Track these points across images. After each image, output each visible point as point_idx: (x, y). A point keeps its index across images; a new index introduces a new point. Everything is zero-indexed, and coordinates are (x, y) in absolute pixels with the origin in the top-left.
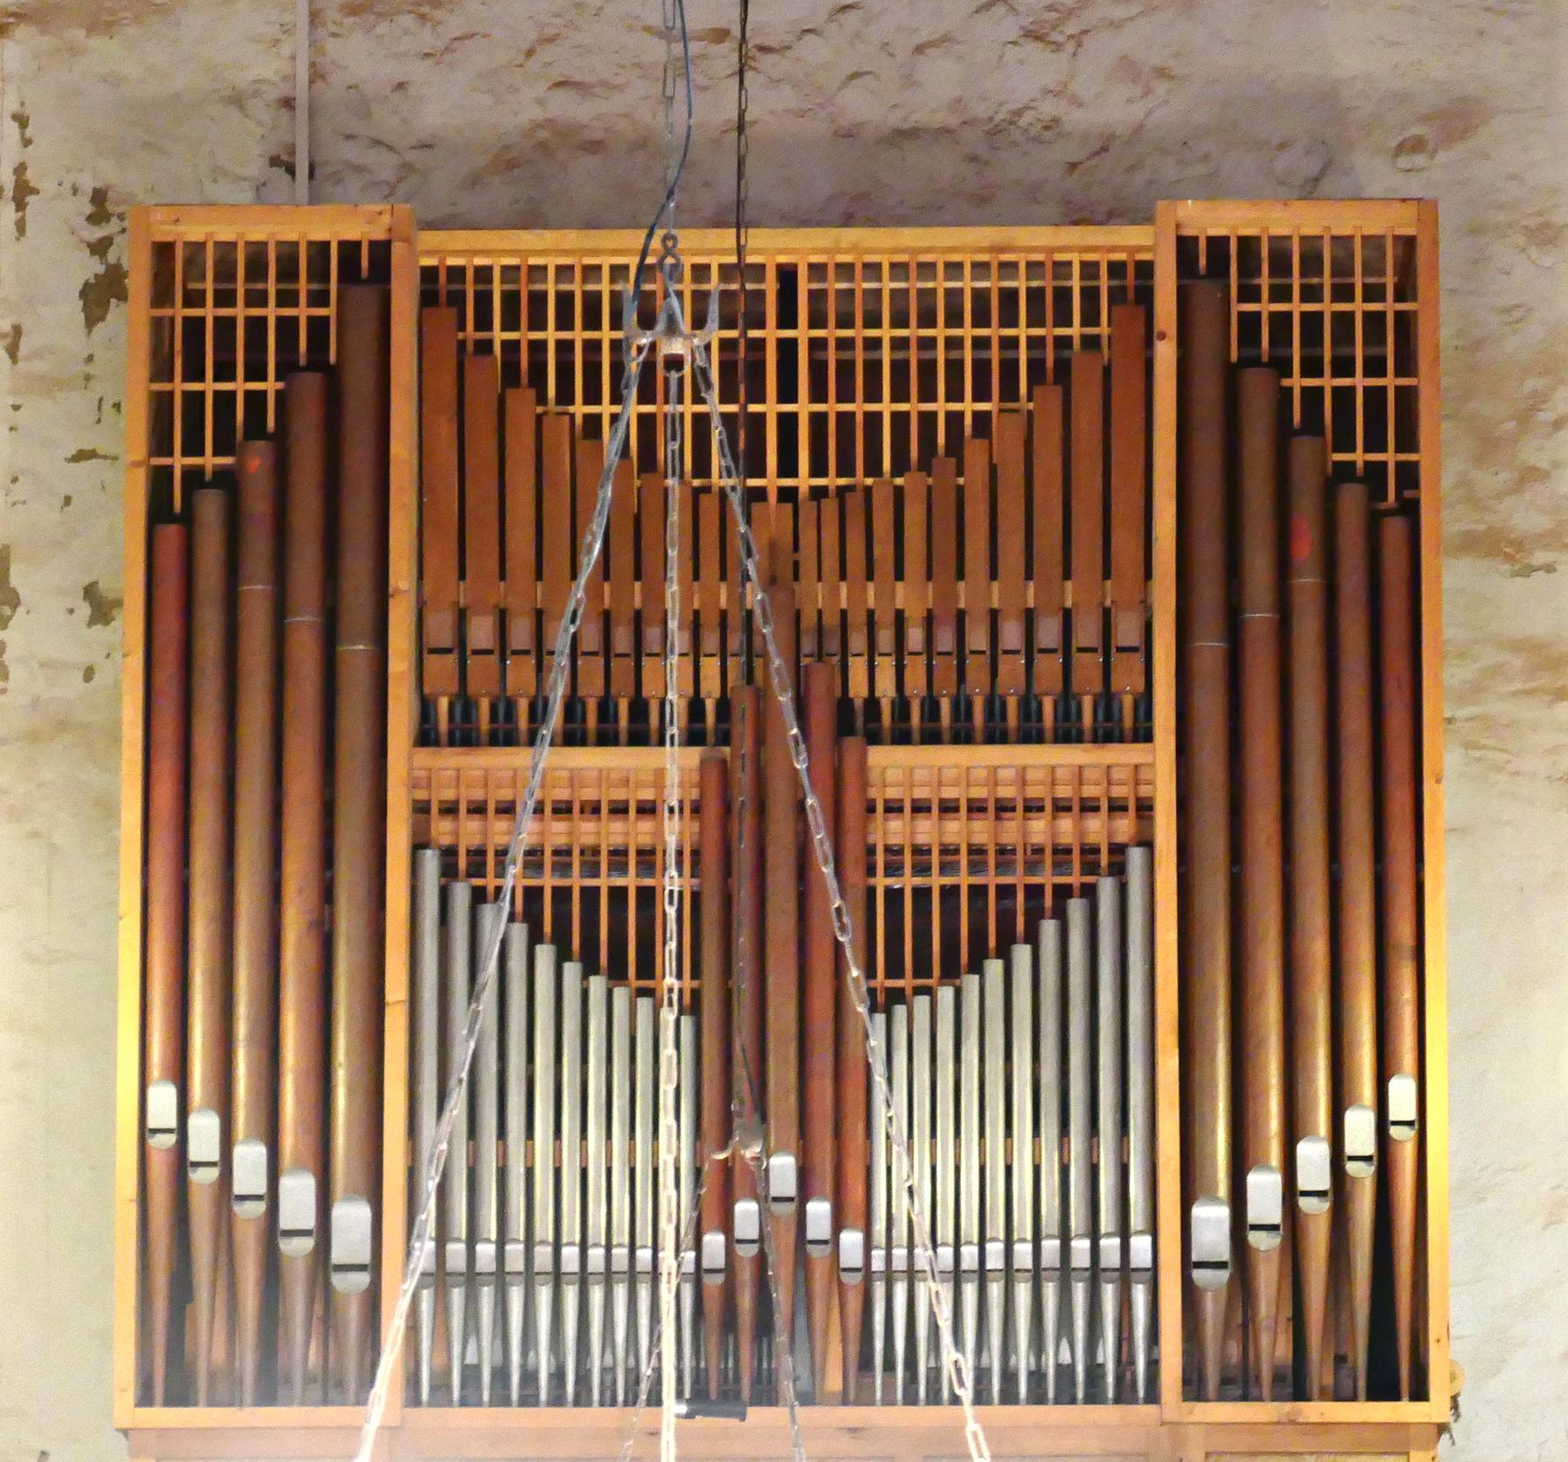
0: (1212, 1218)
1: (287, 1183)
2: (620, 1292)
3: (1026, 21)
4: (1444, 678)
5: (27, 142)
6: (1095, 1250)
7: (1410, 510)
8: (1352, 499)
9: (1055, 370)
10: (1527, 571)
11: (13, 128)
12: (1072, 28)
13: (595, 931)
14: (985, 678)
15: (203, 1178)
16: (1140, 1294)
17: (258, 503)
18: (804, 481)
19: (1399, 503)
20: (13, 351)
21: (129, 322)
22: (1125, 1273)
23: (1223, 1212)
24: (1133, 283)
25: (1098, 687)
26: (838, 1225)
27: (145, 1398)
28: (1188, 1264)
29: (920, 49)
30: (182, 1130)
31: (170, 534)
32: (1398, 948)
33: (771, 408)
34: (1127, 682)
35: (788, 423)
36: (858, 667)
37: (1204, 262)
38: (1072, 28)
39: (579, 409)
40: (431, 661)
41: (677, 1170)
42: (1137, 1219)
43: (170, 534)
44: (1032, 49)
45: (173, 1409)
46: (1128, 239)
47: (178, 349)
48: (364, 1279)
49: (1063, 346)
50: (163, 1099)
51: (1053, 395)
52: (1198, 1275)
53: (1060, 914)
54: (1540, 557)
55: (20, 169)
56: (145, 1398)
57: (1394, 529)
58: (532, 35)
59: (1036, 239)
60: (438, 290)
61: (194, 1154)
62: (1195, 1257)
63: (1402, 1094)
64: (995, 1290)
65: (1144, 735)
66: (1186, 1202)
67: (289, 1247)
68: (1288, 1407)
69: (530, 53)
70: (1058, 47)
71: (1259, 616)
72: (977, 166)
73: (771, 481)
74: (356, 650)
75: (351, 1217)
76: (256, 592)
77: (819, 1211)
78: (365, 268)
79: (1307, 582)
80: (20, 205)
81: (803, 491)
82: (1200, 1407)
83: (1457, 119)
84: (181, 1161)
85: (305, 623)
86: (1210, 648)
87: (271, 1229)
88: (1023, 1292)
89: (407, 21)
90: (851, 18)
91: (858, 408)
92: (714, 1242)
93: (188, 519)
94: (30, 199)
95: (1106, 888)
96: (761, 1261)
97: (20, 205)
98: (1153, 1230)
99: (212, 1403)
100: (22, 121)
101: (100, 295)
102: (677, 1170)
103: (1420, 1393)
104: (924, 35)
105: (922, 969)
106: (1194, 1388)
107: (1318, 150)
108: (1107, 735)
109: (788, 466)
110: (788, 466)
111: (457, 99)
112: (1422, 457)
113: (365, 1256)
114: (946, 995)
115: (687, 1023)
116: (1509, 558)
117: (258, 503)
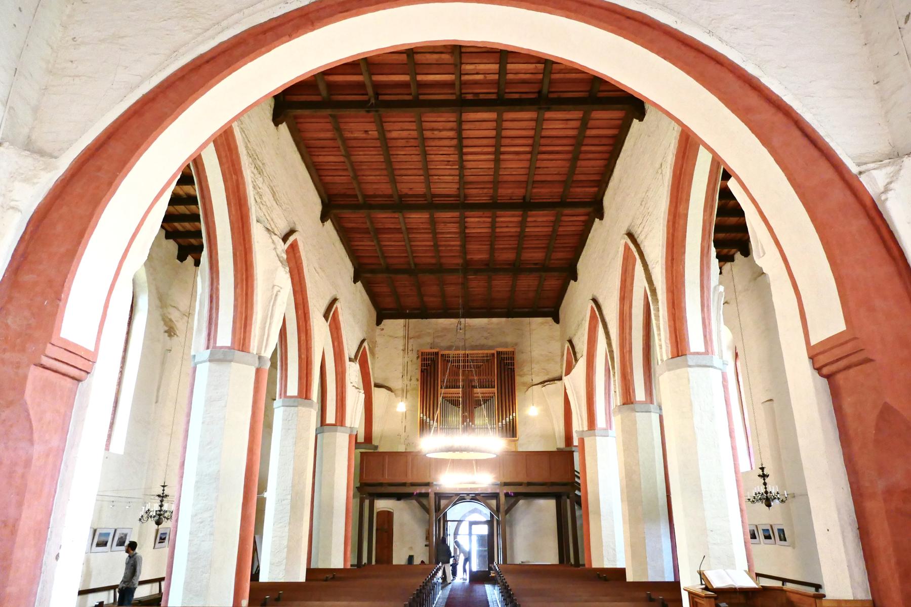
4: (517, 385)
9: (487, 361)
13: (455, 403)
19: (513, 371)
21: (420, 360)
24: (493, 354)
32: (514, 403)
37: (499, 353)
41: (461, 450)
45: (255, 61)
46: (493, 351)
47: (423, 360)
49: (489, 359)
59: (486, 351)
60: (442, 355)
72: (482, 347)
78: (437, 354)
83: (516, 344)
101: (418, 358)
102: (461, 450)
107: (506, 345)
111: (444, 343)
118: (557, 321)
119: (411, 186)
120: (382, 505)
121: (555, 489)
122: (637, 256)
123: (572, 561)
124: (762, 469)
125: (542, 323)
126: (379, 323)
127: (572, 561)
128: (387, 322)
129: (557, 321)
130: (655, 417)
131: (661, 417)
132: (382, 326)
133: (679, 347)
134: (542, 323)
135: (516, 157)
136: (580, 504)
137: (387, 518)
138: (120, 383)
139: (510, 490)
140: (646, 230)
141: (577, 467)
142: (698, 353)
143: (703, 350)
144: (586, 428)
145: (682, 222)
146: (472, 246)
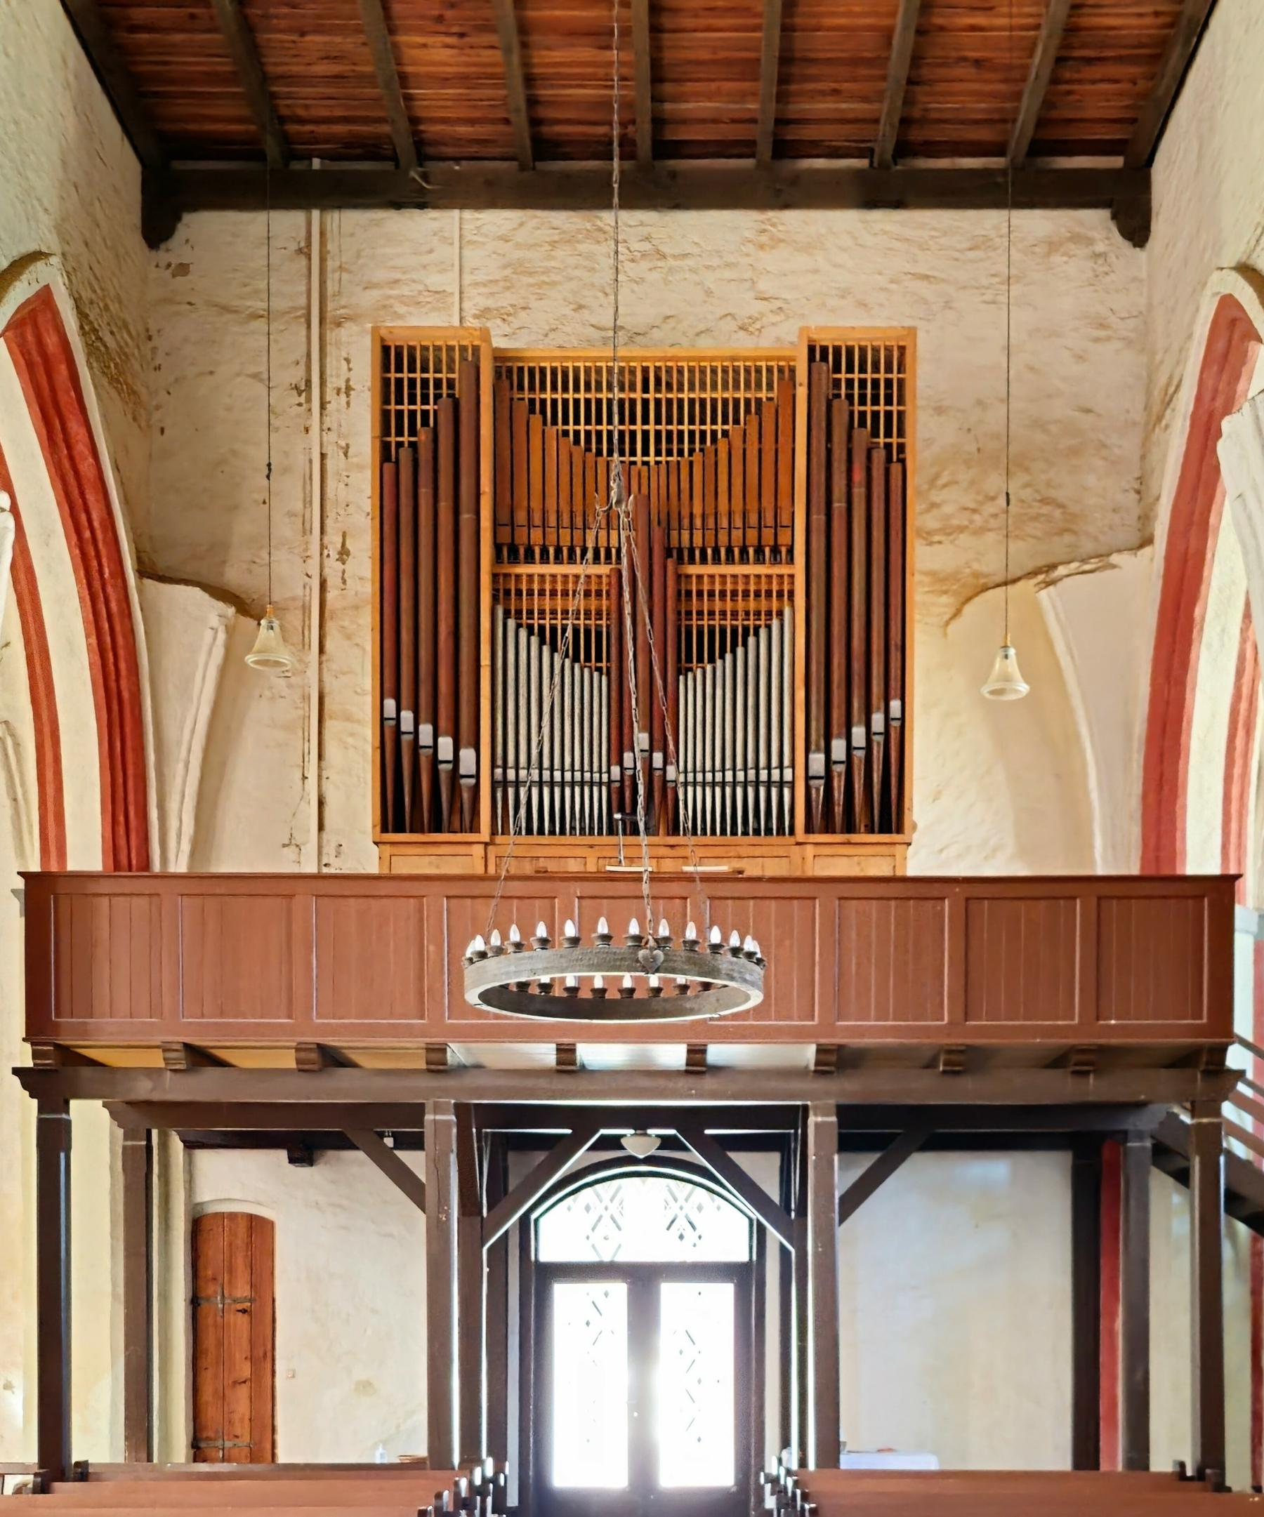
0: (818, 760)
1: (441, 740)
2: (577, 790)
3: (740, 323)
5: (350, 370)
6: (769, 775)
7: (902, 461)
8: (879, 456)
10: (931, 544)
11: (344, 364)
12: (758, 326)
14: (726, 539)
15: (406, 739)
16: (786, 792)
17: (425, 455)
18: (652, 458)
20: (346, 454)
22: (781, 784)
23: (822, 756)
25: (756, 543)
26: (665, 762)
27: (384, 829)
28: (808, 778)
29: (698, 334)
30: (398, 718)
31: (388, 467)
33: (638, 427)
34: (784, 539)
35: (645, 434)
36: (674, 534)
38: (758, 326)
39: (560, 426)
40: (500, 529)
42: (786, 762)
43: (388, 467)
44: (742, 333)
48: (473, 781)
50: (390, 704)
51: (753, 418)
52: (812, 782)
53: (757, 634)
54: (936, 538)
55: (348, 380)
56: (384, 829)
57: (896, 468)
58: (547, 328)
61: (403, 729)
62: (811, 774)
63: (895, 705)
64: (728, 790)
65: (791, 560)
66: (807, 751)
67: (442, 767)
68: (847, 836)
69: (546, 335)
70: (752, 333)
71: (839, 505)
73: (639, 458)
74: (466, 517)
75: (467, 755)
76: (425, 492)
77: (658, 758)
79: (859, 492)
80: (348, 396)
81: (652, 463)
82: (811, 836)
84: (398, 732)
85: (445, 506)
86: (819, 519)
87: (435, 761)
88: (739, 791)
89: (499, 321)
90: (672, 322)
91: (673, 427)
92: (616, 770)
93: (397, 462)
94: (352, 392)
95: (775, 623)
96: (634, 777)
97: (348, 396)
98: (793, 766)
99: (411, 831)
100: (348, 361)
103: (900, 830)
104: (698, 330)
105: (700, 660)
106: (809, 829)
108: (776, 560)
109: (646, 452)
110: (646, 452)
112: (907, 441)
113: (474, 772)
114: (699, 673)
115: (604, 678)
116: (924, 539)
117: (425, 455)
118: (1136, 228)
120: (234, 1180)
125: (1053, 246)
126: (158, 226)
129: (1136, 228)
134: (1053, 246)
137: (232, 1259)
139: (851, 1088)
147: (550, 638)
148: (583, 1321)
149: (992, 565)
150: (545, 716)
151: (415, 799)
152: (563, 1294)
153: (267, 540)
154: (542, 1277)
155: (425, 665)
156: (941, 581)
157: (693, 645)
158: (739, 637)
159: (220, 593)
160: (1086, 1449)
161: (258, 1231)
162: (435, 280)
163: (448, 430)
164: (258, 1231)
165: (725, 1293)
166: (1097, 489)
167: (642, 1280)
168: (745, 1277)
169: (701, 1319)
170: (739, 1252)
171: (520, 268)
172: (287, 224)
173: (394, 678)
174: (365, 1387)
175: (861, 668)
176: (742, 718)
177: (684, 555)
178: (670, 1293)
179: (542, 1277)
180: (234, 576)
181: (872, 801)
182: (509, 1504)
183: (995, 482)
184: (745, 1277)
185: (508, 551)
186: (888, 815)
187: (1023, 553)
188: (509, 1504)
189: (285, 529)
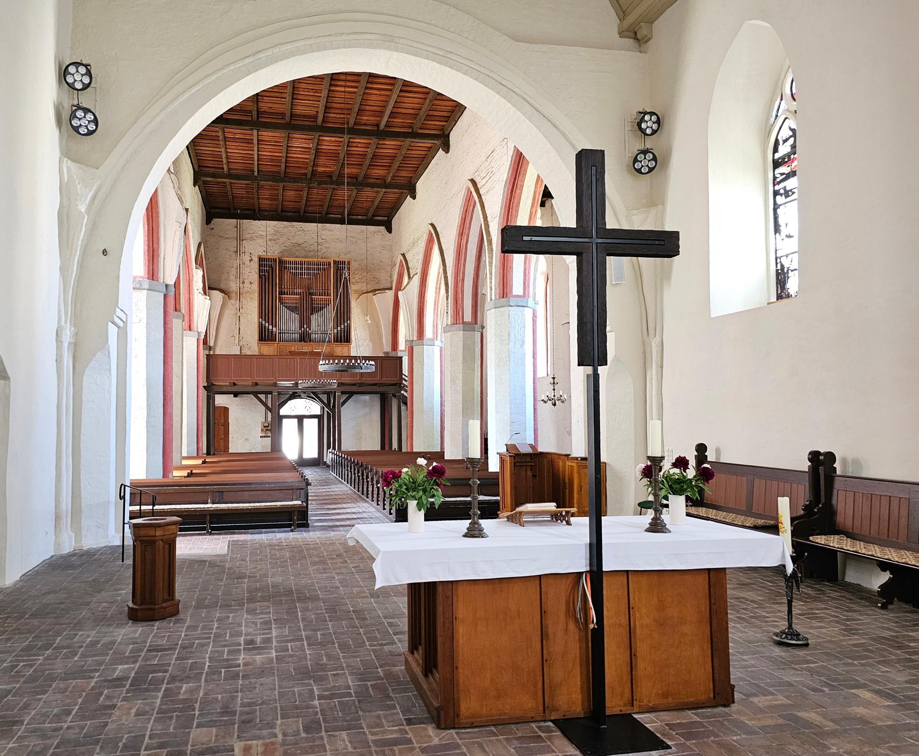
118: (389, 230)
119: (271, 105)
120: (221, 400)
121: (382, 389)
122: (478, 204)
123: (395, 446)
124: (554, 378)
127: (395, 446)
128: (216, 221)
129: (389, 230)
130: (478, 335)
131: (482, 334)
132: (211, 225)
133: (505, 290)
135: (378, 92)
136: (406, 404)
138: (663, 441)
140: (488, 185)
141: (405, 371)
142: (518, 296)
143: (521, 293)
144: (415, 339)
145: (518, 191)
146: (322, 160)
147: (288, 308)
148: (289, 427)
149: (365, 289)
150: (288, 322)
151: (265, 336)
152: (284, 421)
153: (228, 279)
154: (281, 418)
155: (266, 313)
156: (356, 291)
157: (314, 310)
158: (322, 309)
159: (222, 291)
160: (383, 447)
161: (226, 410)
162: (261, 233)
163: (271, 271)
164: (226, 410)
165: (316, 420)
166: (383, 277)
167: (300, 419)
168: (320, 418)
169: (311, 426)
170: (318, 412)
171: (277, 232)
172: (233, 221)
173: (261, 316)
174: (247, 439)
175: (343, 315)
176: (322, 323)
177: (311, 294)
178: (305, 420)
179: (281, 418)
180: (222, 286)
181: (345, 338)
182: (787, 499)
183: (365, 274)
184: (320, 418)
185: (281, 293)
186: (347, 340)
187: (370, 288)
188: (787, 499)
189: (232, 278)
